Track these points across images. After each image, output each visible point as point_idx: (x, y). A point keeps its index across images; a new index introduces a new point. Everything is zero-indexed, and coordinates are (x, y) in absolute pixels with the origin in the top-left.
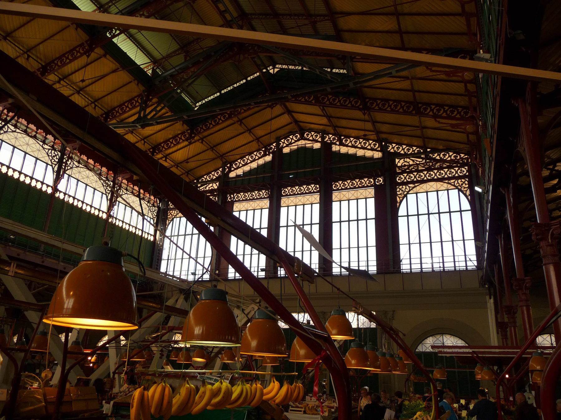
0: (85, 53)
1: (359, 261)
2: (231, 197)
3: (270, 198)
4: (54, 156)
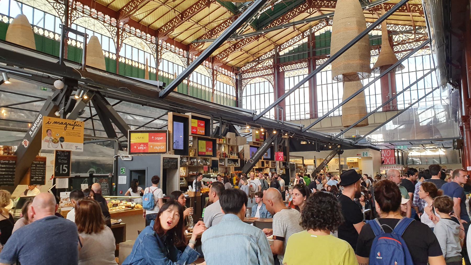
0: (256, 39)
1: (290, 113)
2: (282, 68)
3: (309, 67)
4: (60, 9)
